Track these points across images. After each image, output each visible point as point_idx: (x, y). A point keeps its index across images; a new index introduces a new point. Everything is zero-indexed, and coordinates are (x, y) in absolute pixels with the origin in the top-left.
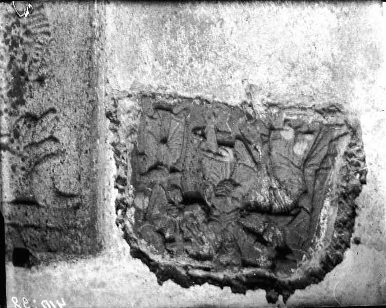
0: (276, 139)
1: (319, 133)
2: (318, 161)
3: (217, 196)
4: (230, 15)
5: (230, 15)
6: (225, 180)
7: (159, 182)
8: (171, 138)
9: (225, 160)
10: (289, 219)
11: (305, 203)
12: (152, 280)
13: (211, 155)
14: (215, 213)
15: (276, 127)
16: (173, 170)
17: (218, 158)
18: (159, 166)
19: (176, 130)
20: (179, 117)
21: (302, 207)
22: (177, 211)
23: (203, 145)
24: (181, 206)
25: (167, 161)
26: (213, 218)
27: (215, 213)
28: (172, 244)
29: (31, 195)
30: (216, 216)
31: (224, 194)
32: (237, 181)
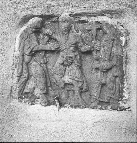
0: (43, 89)
1: (22, 93)
2: (21, 79)
3: (72, 58)
4: (23, 38)
5: (23, 38)
6: (68, 66)
7: (106, 61)
8: (98, 87)
9: (70, 77)
10: (34, 49)
11: (27, 58)
12: (33, 106)
13: (77, 79)
14: (72, 48)
15: (44, 95)
16: (97, 69)
17: (73, 77)
18: (105, 71)
19: (96, 91)
20: (95, 98)
21: (28, 56)
22: (94, 47)
23: (81, 84)
24: (92, 50)
25: (101, 74)
26: (74, 46)
27: (72, 48)
28: (97, 27)
29: (23, 97)
30: (71, 47)
31: (68, 59)
32: (62, 66)
